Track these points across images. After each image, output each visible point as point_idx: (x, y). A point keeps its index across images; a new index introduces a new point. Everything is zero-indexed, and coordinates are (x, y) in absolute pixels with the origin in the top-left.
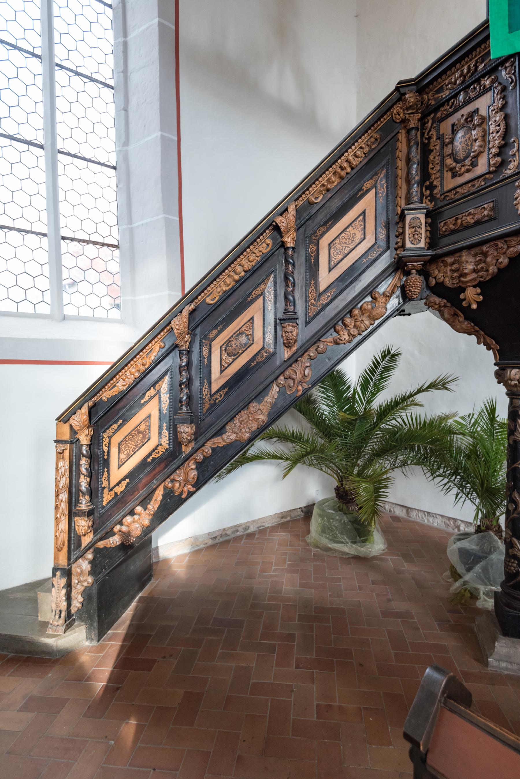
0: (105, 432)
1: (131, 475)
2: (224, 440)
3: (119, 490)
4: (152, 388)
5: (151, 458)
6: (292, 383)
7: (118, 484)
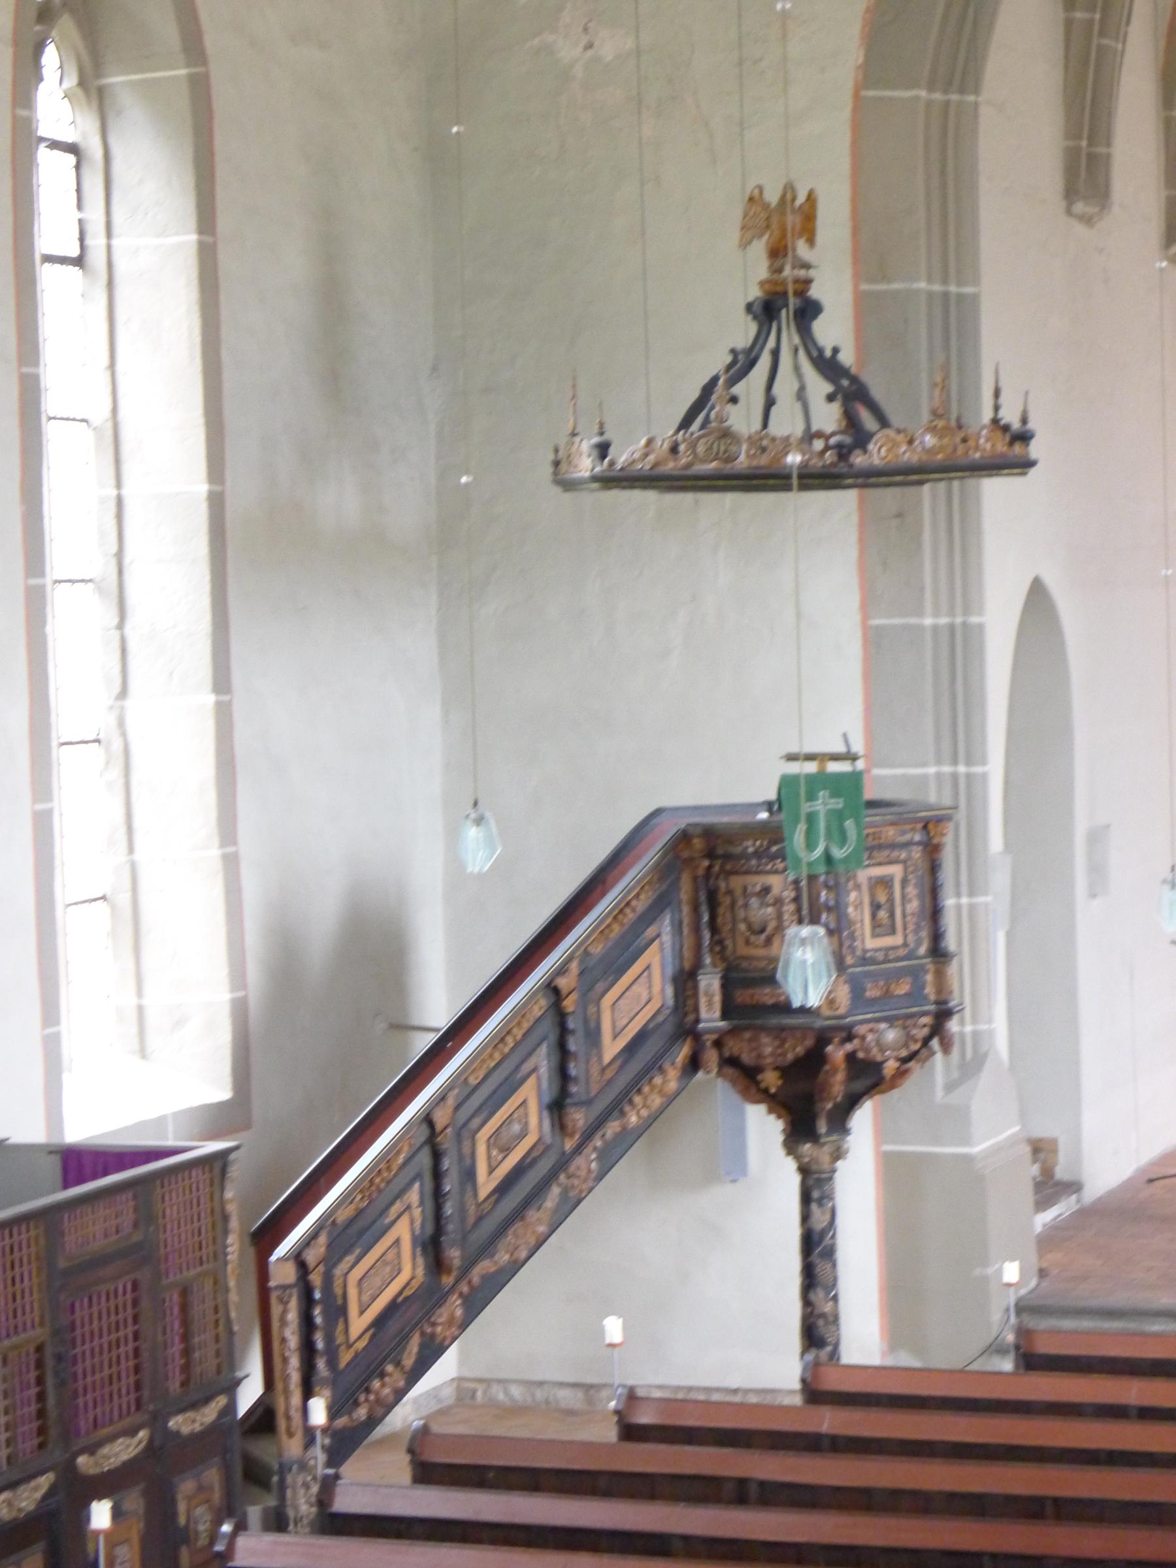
1: (379, 1322)
2: (496, 1263)
3: (361, 1345)
6: (576, 1182)
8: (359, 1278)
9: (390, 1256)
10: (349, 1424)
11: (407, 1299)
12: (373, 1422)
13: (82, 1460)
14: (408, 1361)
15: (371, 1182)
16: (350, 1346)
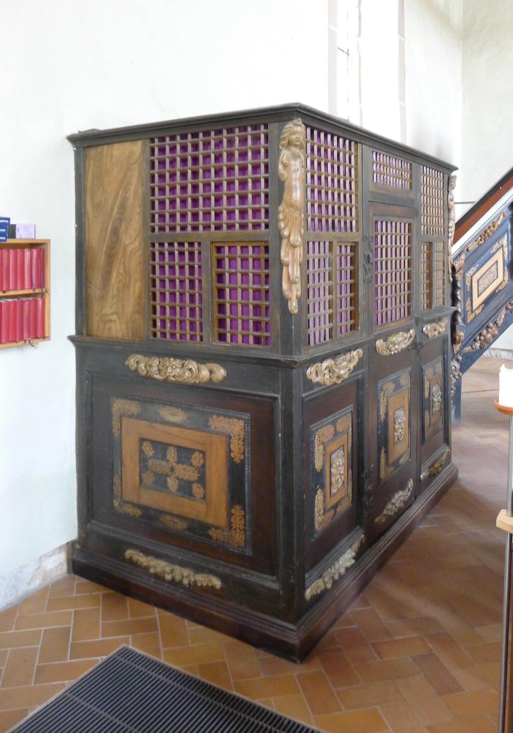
0: (507, 284)
1: (486, 302)
4: (477, 314)
5: (498, 290)
7: (478, 308)
8: (478, 279)
9: (494, 269)
10: (472, 351)
11: (500, 291)
12: (482, 349)
13: (379, 343)
14: (500, 322)
15: (485, 232)
16: (472, 312)
